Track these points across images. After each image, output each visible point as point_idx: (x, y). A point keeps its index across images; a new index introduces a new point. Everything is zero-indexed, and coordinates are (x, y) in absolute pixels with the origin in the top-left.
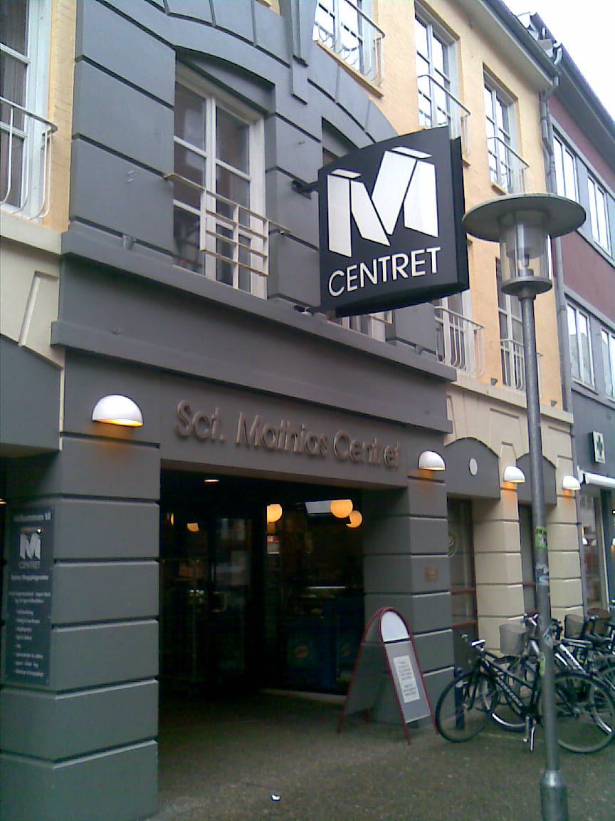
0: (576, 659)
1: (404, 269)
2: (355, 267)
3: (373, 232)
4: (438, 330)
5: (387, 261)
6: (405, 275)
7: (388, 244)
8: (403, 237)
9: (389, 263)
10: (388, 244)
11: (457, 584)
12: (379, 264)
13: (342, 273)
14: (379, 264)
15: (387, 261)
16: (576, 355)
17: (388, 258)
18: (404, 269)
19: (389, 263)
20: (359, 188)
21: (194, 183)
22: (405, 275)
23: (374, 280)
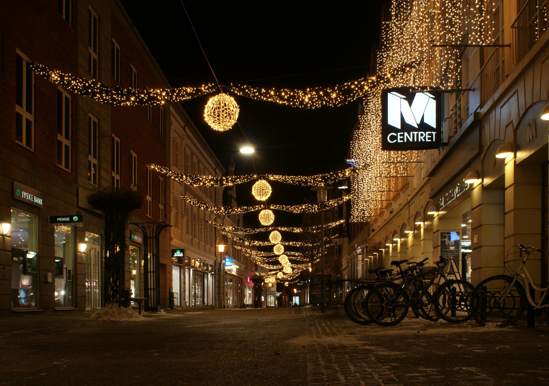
0: (386, 368)
1: (423, 138)
2: (402, 133)
3: (413, 122)
4: (534, 121)
5: (417, 134)
6: (423, 140)
7: (417, 128)
8: (423, 126)
9: (417, 135)
10: (417, 128)
11: (325, 367)
12: (413, 135)
13: (395, 135)
14: (413, 135)
15: (417, 134)
16: (407, 206)
17: (417, 133)
18: (423, 138)
19: (417, 135)
20: (406, 103)
21: (472, 55)
22: (423, 140)
23: (411, 140)
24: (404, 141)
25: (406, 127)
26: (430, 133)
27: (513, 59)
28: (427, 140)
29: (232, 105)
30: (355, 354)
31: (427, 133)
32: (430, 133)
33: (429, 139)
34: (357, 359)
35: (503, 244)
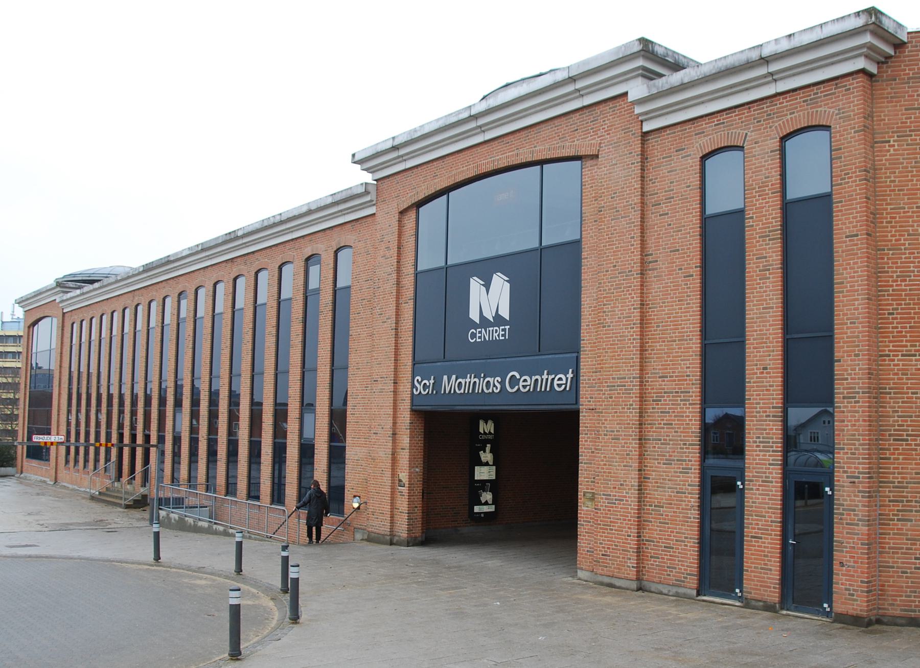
3: (489, 315)
6: (498, 338)
7: (478, 322)
9: (493, 330)
10: (478, 322)
12: (489, 331)
14: (489, 331)
19: (493, 330)
24: (505, 338)
25: (484, 320)
26: (503, 327)
27: (58, 421)
28: (501, 338)
29: (871, 198)
30: (349, 658)
31: (501, 328)
32: (503, 327)
33: (503, 335)
34: (259, 535)
35: (395, 541)
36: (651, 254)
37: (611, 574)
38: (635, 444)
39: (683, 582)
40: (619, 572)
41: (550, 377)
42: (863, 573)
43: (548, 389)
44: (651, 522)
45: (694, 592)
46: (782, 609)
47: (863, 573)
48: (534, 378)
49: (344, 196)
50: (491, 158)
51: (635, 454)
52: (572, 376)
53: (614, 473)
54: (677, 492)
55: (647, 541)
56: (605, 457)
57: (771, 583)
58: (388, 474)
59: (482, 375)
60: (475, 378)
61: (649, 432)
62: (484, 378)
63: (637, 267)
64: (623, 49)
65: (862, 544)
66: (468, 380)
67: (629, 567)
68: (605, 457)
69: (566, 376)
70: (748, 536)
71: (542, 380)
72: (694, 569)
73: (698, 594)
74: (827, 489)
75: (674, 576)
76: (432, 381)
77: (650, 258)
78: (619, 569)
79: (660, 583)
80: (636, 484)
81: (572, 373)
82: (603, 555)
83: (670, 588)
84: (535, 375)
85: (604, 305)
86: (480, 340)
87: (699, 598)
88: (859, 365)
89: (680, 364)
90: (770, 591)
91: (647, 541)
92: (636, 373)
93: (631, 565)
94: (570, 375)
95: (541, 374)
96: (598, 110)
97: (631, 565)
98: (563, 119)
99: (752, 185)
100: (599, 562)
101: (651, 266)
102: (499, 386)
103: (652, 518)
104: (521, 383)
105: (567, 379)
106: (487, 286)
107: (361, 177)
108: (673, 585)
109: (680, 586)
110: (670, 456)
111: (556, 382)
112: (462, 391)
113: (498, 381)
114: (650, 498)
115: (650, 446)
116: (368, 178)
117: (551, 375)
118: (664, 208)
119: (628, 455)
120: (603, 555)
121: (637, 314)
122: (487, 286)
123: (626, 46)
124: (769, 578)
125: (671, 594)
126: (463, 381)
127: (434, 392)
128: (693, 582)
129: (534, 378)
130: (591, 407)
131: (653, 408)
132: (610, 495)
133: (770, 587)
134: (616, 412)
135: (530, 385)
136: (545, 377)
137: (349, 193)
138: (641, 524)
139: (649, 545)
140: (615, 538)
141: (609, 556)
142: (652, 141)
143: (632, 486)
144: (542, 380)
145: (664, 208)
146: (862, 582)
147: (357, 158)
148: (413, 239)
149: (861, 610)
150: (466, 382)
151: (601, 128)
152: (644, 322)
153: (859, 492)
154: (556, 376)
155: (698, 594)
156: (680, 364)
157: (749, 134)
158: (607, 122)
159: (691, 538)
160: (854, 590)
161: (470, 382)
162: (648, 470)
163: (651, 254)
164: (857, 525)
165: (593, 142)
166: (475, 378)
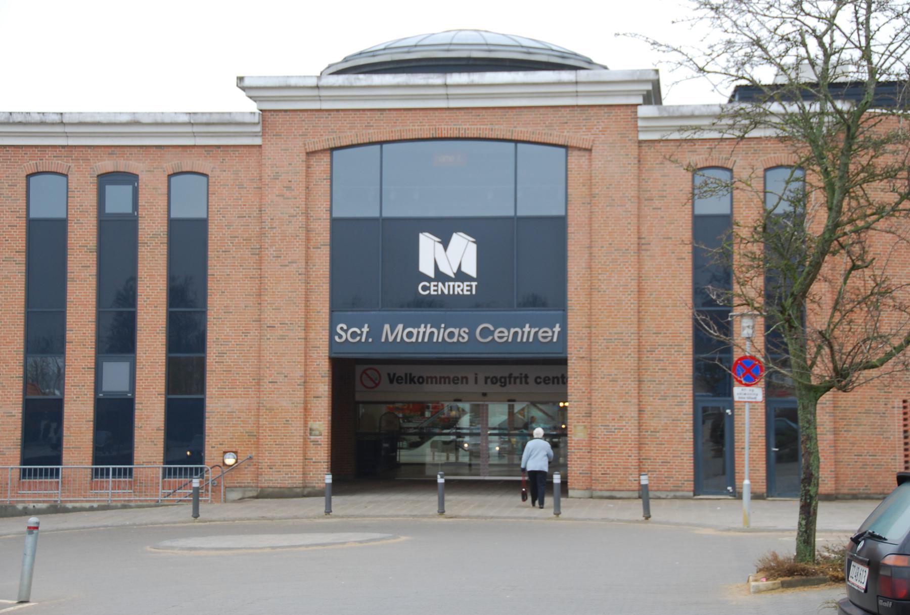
9: (454, 286)
12: (449, 286)
14: (449, 286)
19: (454, 286)
28: (465, 293)
36: (644, 238)
37: (612, 488)
38: (632, 386)
39: (681, 487)
40: (620, 486)
41: (533, 331)
42: (831, 465)
43: (531, 340)
44: (648, 444)
45: (691, 494)
46: (768, 496)
47: (831, 465)
48: (512, 331)
49: (204, 119)
50: (455, 125)
51: (634, 393)
52: (559, 329)
53: (613, 408)
54: (673, 420)
55: (643, 459)
56: (603, 396)
57: (759, 479)
58: (299, 423)
59: (443, 326)
60: (431, 327)
61: (644, 375)
62: (445, 329)
63: (634, 247)
64: (638, 73)
65: (830, 447)
66: (422, 329)
67: (631, 481)
68: (603, 396)
69: (552, 330)
70: (738, 448)
71: (523, 332)
72: (691, 477)
73: (695, 495)
74: (728, 411)
75: (671, 483)
76: (365, 329)
77: (643, 241)
78: (620, 483)
79: (658, 490)
80: (636, 415)
81: (560, 327)
82: (602, 474)
83: (668, 493)
84: (514, 328)
85: (599, 274)
86: (436, 293)
87: (696, 497)
88: (323, 268)
89: (673, 325)
90: (759, 485)
91: (643, 459)
92: (634, 329)
93: (633, 479)
94: (557, 329)
95: (522, 327)
96: (592, 112)
97: (633, 479)
98: (552, 110)
99: (740, 199)
100: (598, 480)
101: (644, 247)
102: (466, 336)
103: (649, 441)
104: (496, 335)
105: (553, 332)
106: (445, 244)
107: (246, 107)
108: (671, 491)
109: (678, 491)
110: (665, 393)
111: (540, 334)
112: (414, 340)
113: (464, 332)
114: (646, 426)
115: (645, 386)
116: (253, 107)
117: (535, 327)
118: (657, 203)
119: (627, 393)
120: (602, 474)
121: (634, 283)
122: (445, 244)
123: (642, 72)
124: (757, 476)
125: (669, 497)
126: (415, 331)
127: (370, 340)
128: (690, 486)
129: (512, 331)
130: (581, 356)
131: (647, 357)
132: (608, 426)
133: (758, 482)
134: (614, 360)
135: (508, 336)
136: (527, 329)
137: (226, 118)
138: (640, 446)
139: (646, 462)
140: (616, 459)
141: (609, 474)
142: (645, 147)
143: (632, 417)
144: (523, 332)
145: (657, 203)
146: (831, 471)
147: (247, 83)
148: (326, 183)
149: (831, 490)
150: (418, 332)
151: (595, 127)
152: (640, 291)
153: (827, 413)
154: (539, 330)
155: (695, 495)
156: (673, 325)
157: (738, 161)
158: (601, 123)
159: (687, 454)
160: (825, 477)
161: (424, 333)
162: (643, 405)
163: (644, 238)
164: (826, 434)
165: (585, 137)
166: (431, 327)
